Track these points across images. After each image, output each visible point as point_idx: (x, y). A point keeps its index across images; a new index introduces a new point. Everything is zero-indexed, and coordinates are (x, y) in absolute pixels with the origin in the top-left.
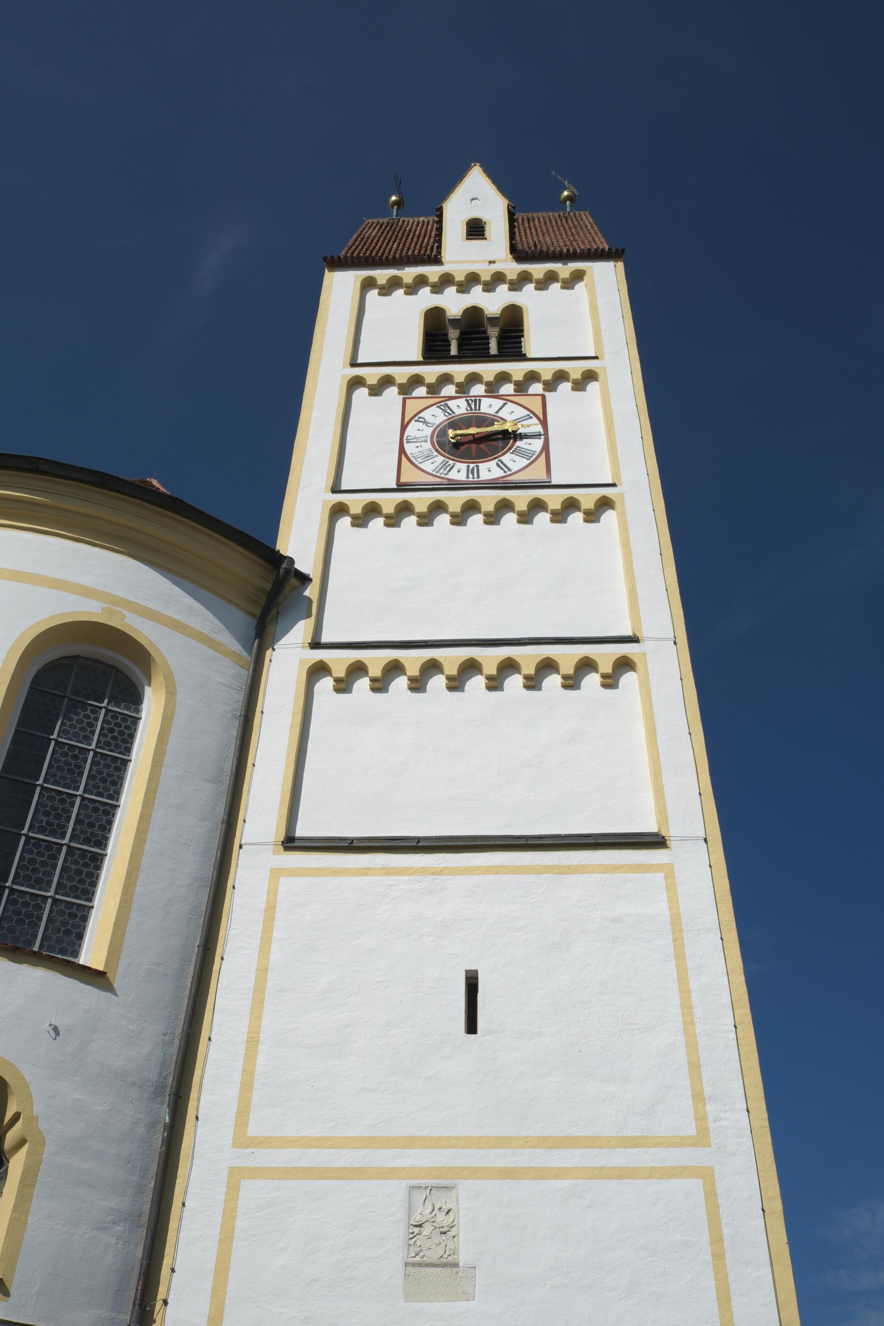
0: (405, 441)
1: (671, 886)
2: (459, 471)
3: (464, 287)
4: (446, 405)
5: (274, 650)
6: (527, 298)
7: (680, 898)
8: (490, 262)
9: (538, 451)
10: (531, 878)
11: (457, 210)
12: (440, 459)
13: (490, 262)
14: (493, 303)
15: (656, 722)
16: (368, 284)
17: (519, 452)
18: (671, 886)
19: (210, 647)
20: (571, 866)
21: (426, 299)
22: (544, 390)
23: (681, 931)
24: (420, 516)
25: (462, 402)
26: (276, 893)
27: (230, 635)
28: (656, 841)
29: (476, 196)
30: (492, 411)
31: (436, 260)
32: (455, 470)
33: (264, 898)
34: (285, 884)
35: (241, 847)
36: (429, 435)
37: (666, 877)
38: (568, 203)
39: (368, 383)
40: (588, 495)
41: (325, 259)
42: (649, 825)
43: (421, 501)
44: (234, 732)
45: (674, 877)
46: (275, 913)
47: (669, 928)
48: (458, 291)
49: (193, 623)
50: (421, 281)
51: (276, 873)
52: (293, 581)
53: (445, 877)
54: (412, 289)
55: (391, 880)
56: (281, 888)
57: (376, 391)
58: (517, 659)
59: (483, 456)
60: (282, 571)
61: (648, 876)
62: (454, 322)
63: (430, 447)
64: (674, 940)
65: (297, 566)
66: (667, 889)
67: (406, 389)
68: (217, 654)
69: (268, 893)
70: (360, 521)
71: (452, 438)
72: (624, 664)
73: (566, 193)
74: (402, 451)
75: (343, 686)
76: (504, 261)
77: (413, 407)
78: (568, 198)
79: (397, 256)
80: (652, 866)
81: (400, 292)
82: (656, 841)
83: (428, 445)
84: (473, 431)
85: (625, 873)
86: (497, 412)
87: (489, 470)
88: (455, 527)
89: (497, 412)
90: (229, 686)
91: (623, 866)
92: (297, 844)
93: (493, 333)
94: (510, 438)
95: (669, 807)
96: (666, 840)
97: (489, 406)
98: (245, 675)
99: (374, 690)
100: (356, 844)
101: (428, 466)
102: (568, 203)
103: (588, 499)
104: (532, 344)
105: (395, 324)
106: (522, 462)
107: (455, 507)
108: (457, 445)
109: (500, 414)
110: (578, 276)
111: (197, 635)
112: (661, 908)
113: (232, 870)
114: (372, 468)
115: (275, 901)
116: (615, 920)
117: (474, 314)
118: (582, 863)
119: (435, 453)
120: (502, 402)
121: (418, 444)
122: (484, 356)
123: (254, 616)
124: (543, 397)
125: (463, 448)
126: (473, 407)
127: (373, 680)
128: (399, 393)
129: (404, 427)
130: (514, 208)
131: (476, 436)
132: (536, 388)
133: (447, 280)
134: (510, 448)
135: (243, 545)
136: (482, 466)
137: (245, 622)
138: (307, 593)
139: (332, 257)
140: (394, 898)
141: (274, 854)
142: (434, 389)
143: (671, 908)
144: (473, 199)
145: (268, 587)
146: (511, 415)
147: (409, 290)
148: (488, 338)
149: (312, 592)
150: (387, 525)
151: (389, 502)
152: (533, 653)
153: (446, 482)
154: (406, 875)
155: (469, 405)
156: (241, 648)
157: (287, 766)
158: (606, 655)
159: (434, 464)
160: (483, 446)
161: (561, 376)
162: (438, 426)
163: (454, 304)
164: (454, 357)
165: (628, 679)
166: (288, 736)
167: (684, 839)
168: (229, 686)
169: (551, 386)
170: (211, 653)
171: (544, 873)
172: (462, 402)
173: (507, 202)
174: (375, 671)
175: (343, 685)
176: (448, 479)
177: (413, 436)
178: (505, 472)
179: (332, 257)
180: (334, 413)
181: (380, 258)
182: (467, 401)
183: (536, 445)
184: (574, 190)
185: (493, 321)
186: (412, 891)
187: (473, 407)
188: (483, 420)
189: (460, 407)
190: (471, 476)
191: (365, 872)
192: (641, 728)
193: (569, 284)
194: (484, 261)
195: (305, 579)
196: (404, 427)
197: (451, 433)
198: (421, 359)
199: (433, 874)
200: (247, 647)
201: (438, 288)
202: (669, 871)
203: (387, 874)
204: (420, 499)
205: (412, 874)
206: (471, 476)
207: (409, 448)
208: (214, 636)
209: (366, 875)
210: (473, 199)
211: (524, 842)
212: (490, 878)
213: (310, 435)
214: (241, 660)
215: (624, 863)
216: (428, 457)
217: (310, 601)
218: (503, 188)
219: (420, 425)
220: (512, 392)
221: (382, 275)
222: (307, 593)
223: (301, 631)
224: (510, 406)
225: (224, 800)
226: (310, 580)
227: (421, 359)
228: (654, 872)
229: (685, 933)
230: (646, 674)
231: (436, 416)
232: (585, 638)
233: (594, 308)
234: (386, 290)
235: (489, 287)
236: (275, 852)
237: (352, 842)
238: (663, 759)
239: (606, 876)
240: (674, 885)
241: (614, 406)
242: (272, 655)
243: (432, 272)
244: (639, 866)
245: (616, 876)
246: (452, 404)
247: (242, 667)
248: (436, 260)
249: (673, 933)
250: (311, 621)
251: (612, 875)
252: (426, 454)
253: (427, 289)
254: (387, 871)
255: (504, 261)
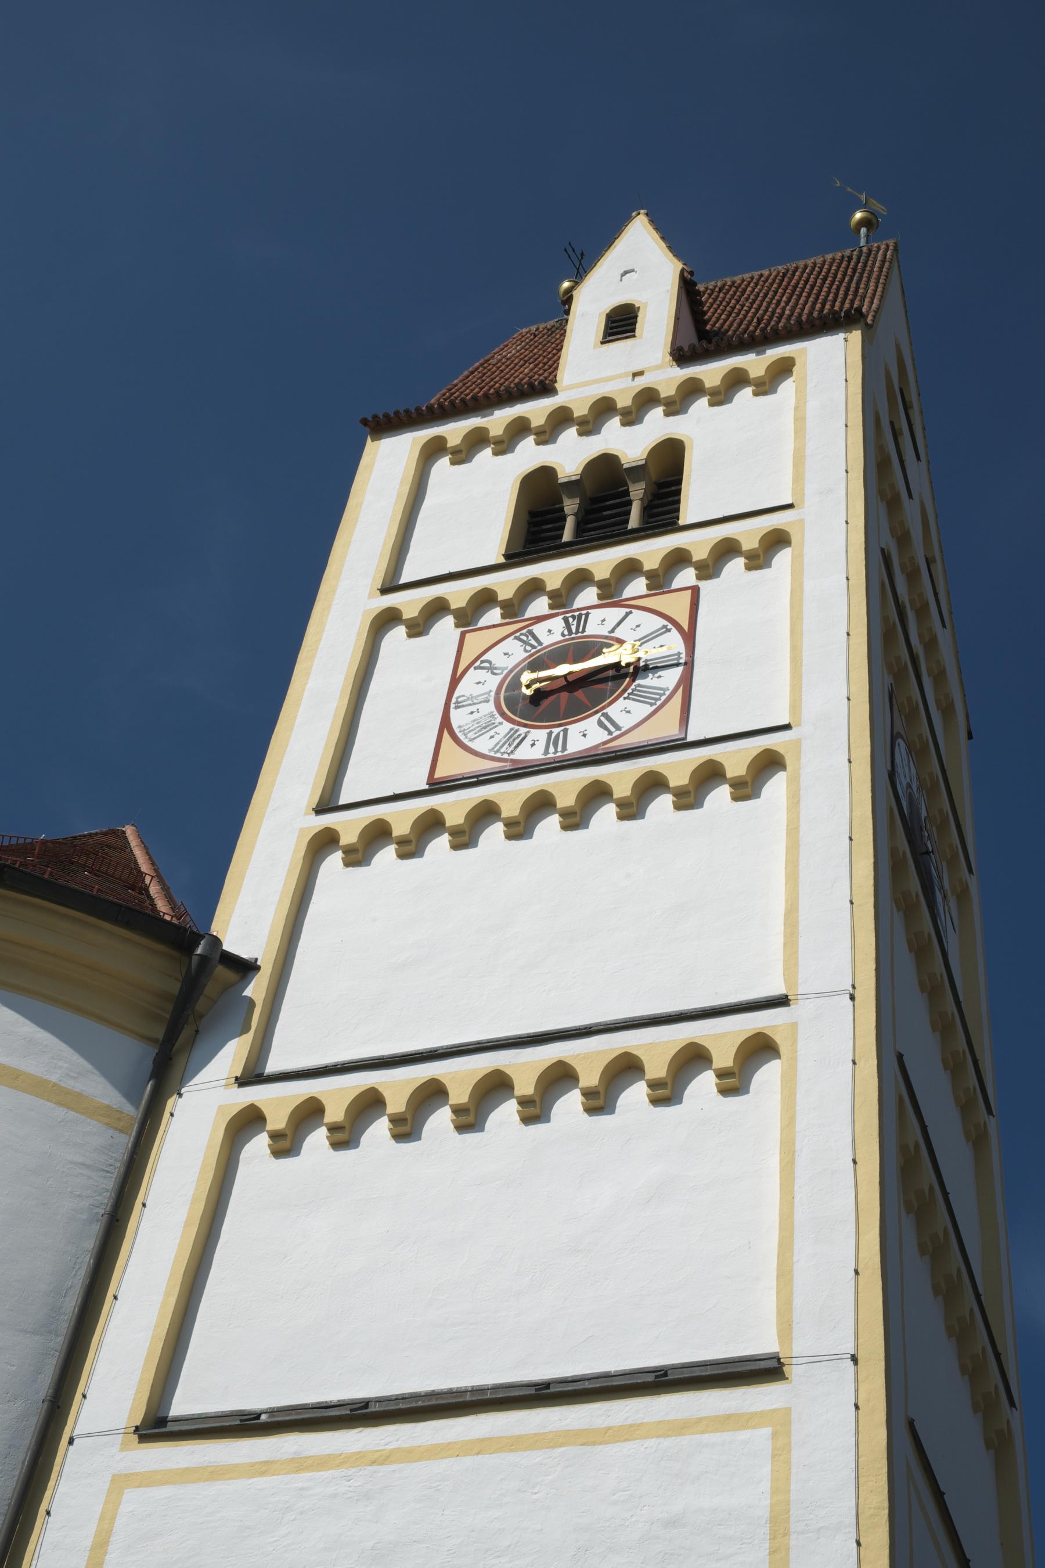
0: (452, 706)
1: (781, 1452)
2: (534, 745)
3: (589, 426)
4: (531, 633)
5: (180, 1095)
6: (698, 427)
7: (793, 1471)
8: (635, 375)
9: (671, 688)
10: (537, 1457)
11: (592, 300)
12: (507, 726)
13: (635, 375)
14: (630, 444)
15: (798, 1147)
16: (434, 450)
17: (638, 697)
18: (781, 1452)
19: (59, 1104)
20: (609, 1429)
21: (529, 455)
22: (699, 577)
23: (786, 1534)
24: (566, 814)
25: (557, 624)
26: (113, 1518)
27: (102, 1079)
28: (766, 1370)
29: (640, 267)
30: (604, 631)
31: (547, 389)
32: (528, 741)
33: (92, 1528)
34: (132, 1500)
35: (71, 1441)
36: (494, 689)
37: (775, 1435)
38: (863, 230)
39: (453, 607)
40: (739, 751)
41: (365, 422)
42: (760, 1343)
43: (454, 806)
44: (90, 1244)
45: (788, 1434)
46: (106, 1553)
47: (766, 1529)
48: (581, 434)
49: (32, 1066)
50: (520, 429)
51: (120, 1483)
52: (221, 972)
53: (393, 1467)
54: (504, 445)
55: (303, 1479)
56: (125, 1508)
57: (418, 628)
58: (508, 1072)
59: (577, 711)
60: (195, 960)
61: (743, 1435)
62: (573, 487)
63: (493, 709)
64: (772, 1552)
65: (226, 947)
66: (773, 1456)
67: (467, 618)
68: (72, 1114)
69: (102, 1519)
70: (358, 856)
71: (528, 686)
72: (760, 1049)
73: (858, 215)
74: (446, 723)
75: (286, 1145)
76: (658, 367)
77: (475, 642)
78: (862, 223)
79: (804, 318)
80: (753, 1415)
81: (746, 393)
82: (766, 1370)
83: (490, 707)
84: (562, 670)
85: (702, 1432)
86: (613, 631)
87: (584, 734)
88: (513, 842)
89: (613, 631)
90: (88, 1167)
91: (700, 1420)
92: (171, 1427)
93: (637, 492)
94: (625, 676)
95: (797, 1301)
96: (782, 1365)
97: (600, 622)
98: (125, 1141)
99: (591, 1110)
100: (374, 1408)
101: (483, 745)
102: (863, 230)
103: (736, 759)
104: (693, 505)
105: (472, 505)
106: (642, 710)
107: (622, 789)
108: (539, 696)
109: (618, 634)
110: (783, 369)
111: (39, 1087)
112: (757, 1498)
113: (51, 1483)
114: (391, 761)
115: (109, 1532)
116: (673, 1523)
117: (605, 466)
118: (629, 1422)
119: (500, 719)
120: (623, 611)
121: (473, 708)
122: (622, 535)
123: (154, 1041)
124: (695, 591)
125: (545, 703)
126: (574, 628)
127: (721, 1074)
128: (457, 626)
129: (455, 681)
130: (691, 273)
131: (570, 679)
132: (687, 577)
133: (561, 419)
134: (625, 690)
135: (127, 925)
136: (574, 729)
137: (135, 1053)
138: (248, 992)
139: (375, 417)
140: (302, 1513)
141: (122, 1450)
142: (513, 609)
143: (774, 1491)
144: (626, 273)
145: (174, 987)
146: (629, 633)
147: (500, 447)
148: (630, 503)
149: (256, 989)
150: (402, 856)
151: (402, 818)
152: (601, 1048)
153: (508, 766)
154: (330, 1469)
155: (568, 626)
156: (123, 1100)
157: (167, 1294)
158: (722, 1038)
159: (491, 737)
160: (580, 694)
161: (727, 550)
162: (511, 671)
163: (570, 456)
164: (634, 531)
165: (768, 1076)
166: (177, 1241)
167: (816, 1360)
168: (88, 1167)
169: (709, 569)
170: (60, 1112)
171: (561, 1445)
172: (557, 624)
173: (680, 266)
174: (724, 1057)
175: (470, 1119)
176: (513, 761)
177: (468, 694)
178: (610, 733)
179: (375, 417)
180: (342, 677)
181: (848, 312)
182: (566, 620)
183: (671, 678)
184: (880, 208)
185: (637, 472)
186: (334, 1496)
187: (574, 628)
188: (593, 648)
189: (552, 632)
190: (552, 749)
191: (264, 1468)
192: (774, 1162)
193: (766, 386)
194: (626, 374)
195: (246, 968)
196: (455, 681)
197: (526, 677)
198: (502, 560)
199: (374, 1463)
200: (131, 1095)
201: (547, 435)
202: (781, 1423)
203: (298, 1470)
204: (455, 803)
205: (338, 1466)
206: (552, 749)
207: (458, 718)
208: (70, 1084)
209: (263, 1473)
210: (626, 273)
211: (650, 1378)
212: (468, 1461)
213: (298, 720)
214: (119, 1119)
215: (704, 1414)
216: (488, 727)
217: (251, 1003)
218: (675, 248)
219: (482, 675)
220: (595, 601)
221: (454, 431)
222: (248, 992)
223: (231, 1056)
224: (637, 615)
225: (54, 1361)
226: (258, 968)
227: (502, 560)
228: (754, 1427)
229: (793, 1537)
230: (794, 1059)
231: (510, 654)
232: (625, 1021)
233: (800, 419)
234: (462, 455)
235: (632, 417)
236: (124, 1447)
237: (666, 1374)
238: (799, 1216)
239: (667, 1442)
240: (787, 1447)
241: (809, 585)
242: (174, 1105)
243: (536, 410)
244: (728, 1417)
245: (687, 1441)
246: (539, 629)
247: (121, 1131)
248: (547, 389)
249: (773, 1538)
250: (248, 1038)
251: (679, 1438)
252: (483, 723)
253: (531, 440)
254: (300, 1464)
255: (658, 367)
